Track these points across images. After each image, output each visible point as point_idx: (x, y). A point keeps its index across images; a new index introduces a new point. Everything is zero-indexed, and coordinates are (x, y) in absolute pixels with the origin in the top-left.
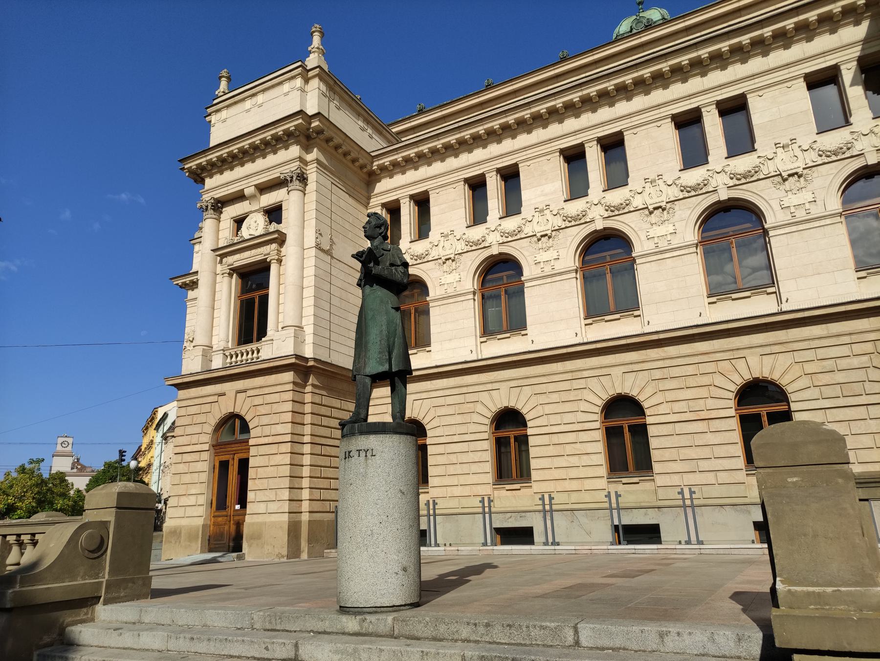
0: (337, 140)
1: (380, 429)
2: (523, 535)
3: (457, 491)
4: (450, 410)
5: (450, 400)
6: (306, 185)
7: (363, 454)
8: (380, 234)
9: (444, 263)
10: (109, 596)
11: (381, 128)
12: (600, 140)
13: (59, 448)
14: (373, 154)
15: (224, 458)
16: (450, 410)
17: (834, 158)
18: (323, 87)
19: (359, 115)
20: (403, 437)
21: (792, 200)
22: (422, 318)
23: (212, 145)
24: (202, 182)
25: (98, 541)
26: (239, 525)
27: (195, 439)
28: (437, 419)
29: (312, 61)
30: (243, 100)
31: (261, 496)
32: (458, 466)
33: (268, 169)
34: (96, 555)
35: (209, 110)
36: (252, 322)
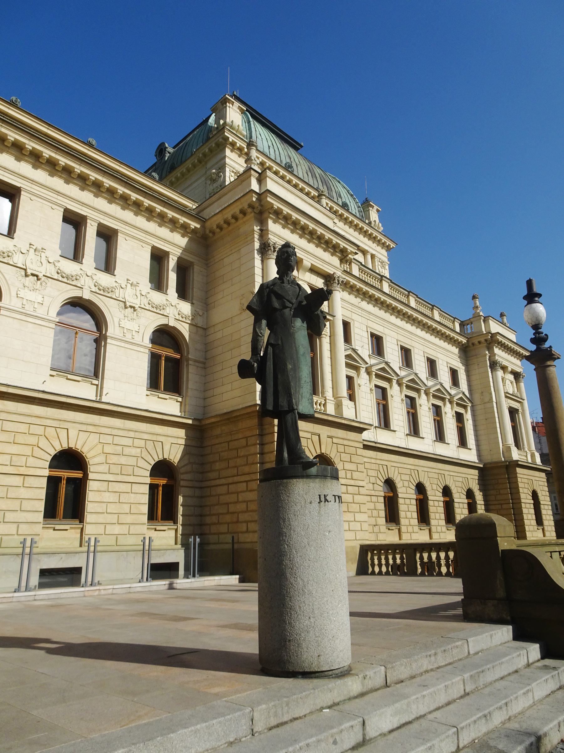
2: (71, 576)
12: (100, 225)
17: (155, 310)
21: (127, 324)
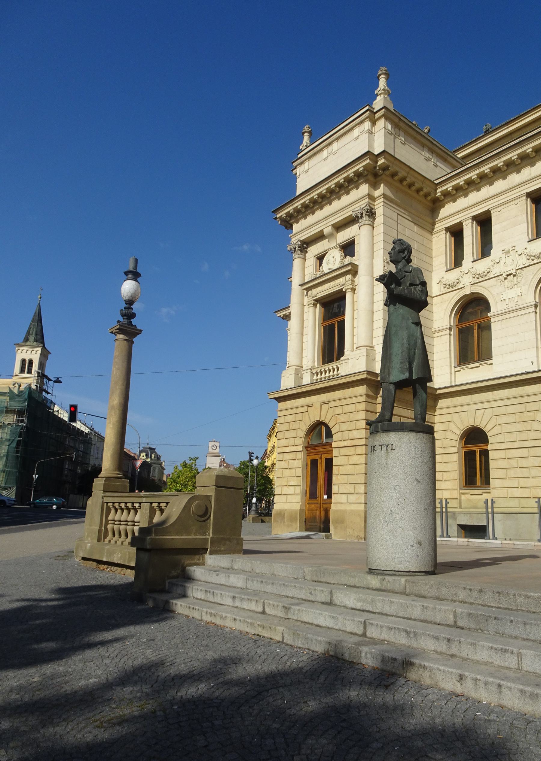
0: (402, 174)
1: (401, 428)
3: (517, 493)
4: (511, 419)
5: (510, 409)
6: (374, 219)
7: (384, 448)
8: (404, 258)
9: (505, 279)
10: (213, 549)
11: (445, 156)
13: (210, 450)
14: (436, 182)
15: (314, 457)
16: (511, 419)
18: (389, 126)
19: (423, 146)
20: (419, 435)
22: (485, 333)
23: (298, 193)
24: (291, 227)
25: (204, 509)
26: (327, 511)
27: (292, 442)
28: (498, 427)
29: (379, 103)
30: (321, 150)
31: (343, 489)
32: (518, 470)
33: (342, 209)
34: (203, 519)
35: (295, 164)
36: (332, 345)
